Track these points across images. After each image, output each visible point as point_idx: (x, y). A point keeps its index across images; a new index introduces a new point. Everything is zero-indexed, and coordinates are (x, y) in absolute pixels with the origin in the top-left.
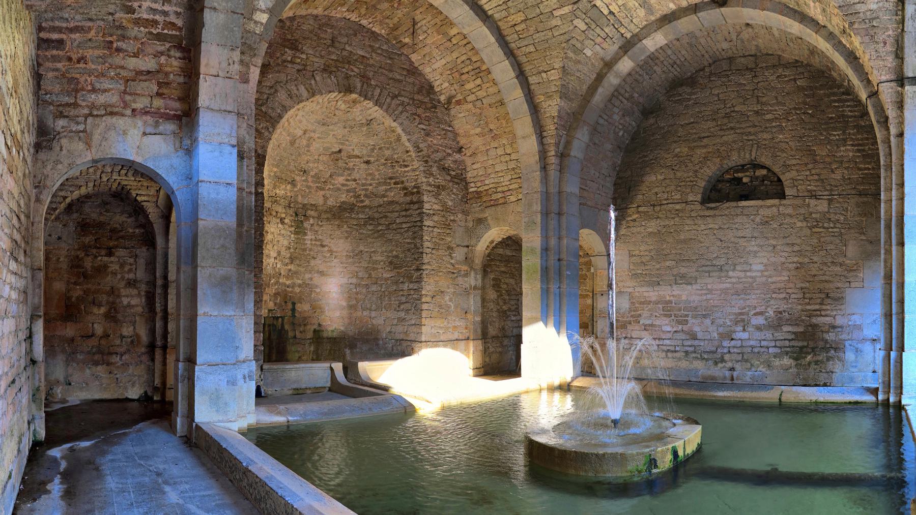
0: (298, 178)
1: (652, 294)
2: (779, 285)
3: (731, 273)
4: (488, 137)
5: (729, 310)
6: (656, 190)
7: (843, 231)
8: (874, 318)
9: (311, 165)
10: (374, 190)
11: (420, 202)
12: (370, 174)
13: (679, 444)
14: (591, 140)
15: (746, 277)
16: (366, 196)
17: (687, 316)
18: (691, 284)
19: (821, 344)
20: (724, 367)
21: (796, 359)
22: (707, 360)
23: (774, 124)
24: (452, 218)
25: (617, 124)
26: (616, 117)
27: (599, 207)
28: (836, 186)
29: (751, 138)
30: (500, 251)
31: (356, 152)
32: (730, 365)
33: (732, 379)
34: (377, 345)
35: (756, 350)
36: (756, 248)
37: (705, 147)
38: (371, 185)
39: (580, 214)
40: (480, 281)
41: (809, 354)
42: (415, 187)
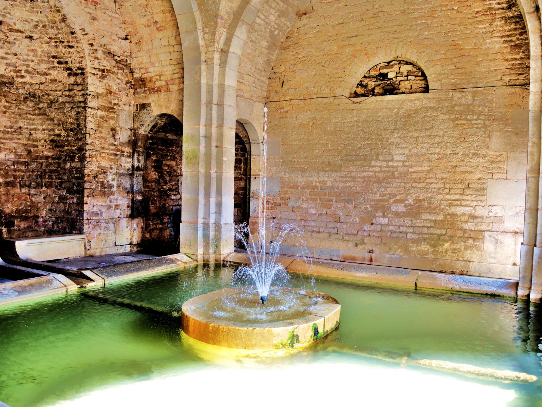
1: (300, 179)
2: (419, 175)
3: (373, 163)
4: (154, 28)
5: (370, 196)
6: (306, 85)
7: (487, 123)
8: (517, 210)
10: (36, 67)
11: (84, 84)
12: (32, 50)
13: (319, 322)
14: (249, 37)
15: (387, 166)
16: (27, 71)
17: (331, 200)
18: (336, 172)
19: (459, 233)
20: (364, 249)
21: (433, 246)
22: (348, 241)
23: (419, 22)
24: (116, 102)
25: (273, 24)
26: (273, 18)
27: (254, 99)
28: (481, 79)
29: (396, 36)
30: (161, 135)
31: (18, 26)
32: (369, 247)
33: (371, 260)
34: (37, 222)
35: (395, 235)
36: (398, 140)
37: (353, 45)
38: (33, 61)
39: (237, 105)
40: (142, 162)
41: (447, 241)
42: (79, 68)
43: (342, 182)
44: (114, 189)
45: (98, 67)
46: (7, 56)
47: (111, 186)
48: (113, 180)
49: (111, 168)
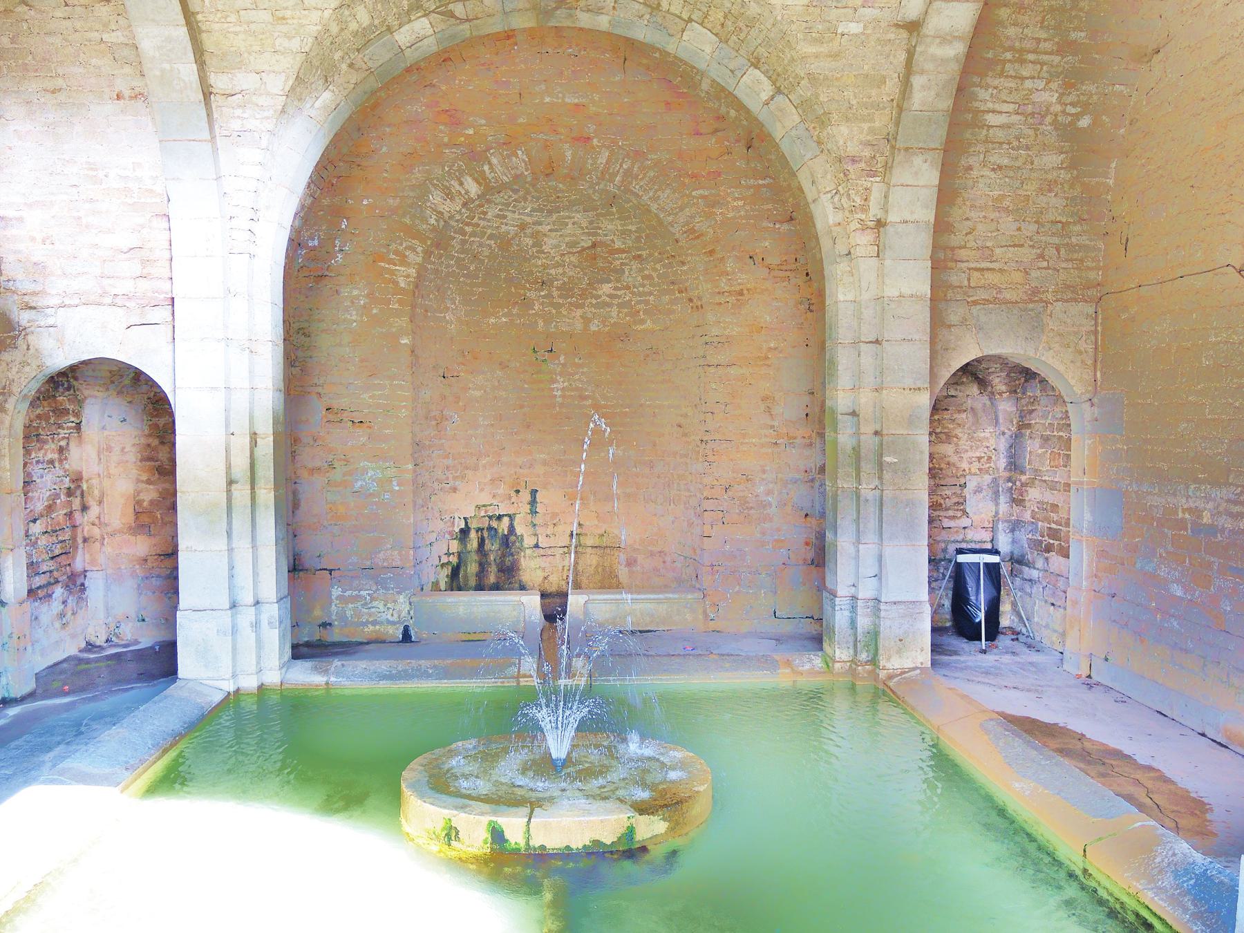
0: (532, 295)
9: (553, 272)
43: (1231, 515)
44: (773, 510)
45: (727, 288)
46: (619, 293)
47: (764, 505)
48: (769, 493)
49: (764, 472)
